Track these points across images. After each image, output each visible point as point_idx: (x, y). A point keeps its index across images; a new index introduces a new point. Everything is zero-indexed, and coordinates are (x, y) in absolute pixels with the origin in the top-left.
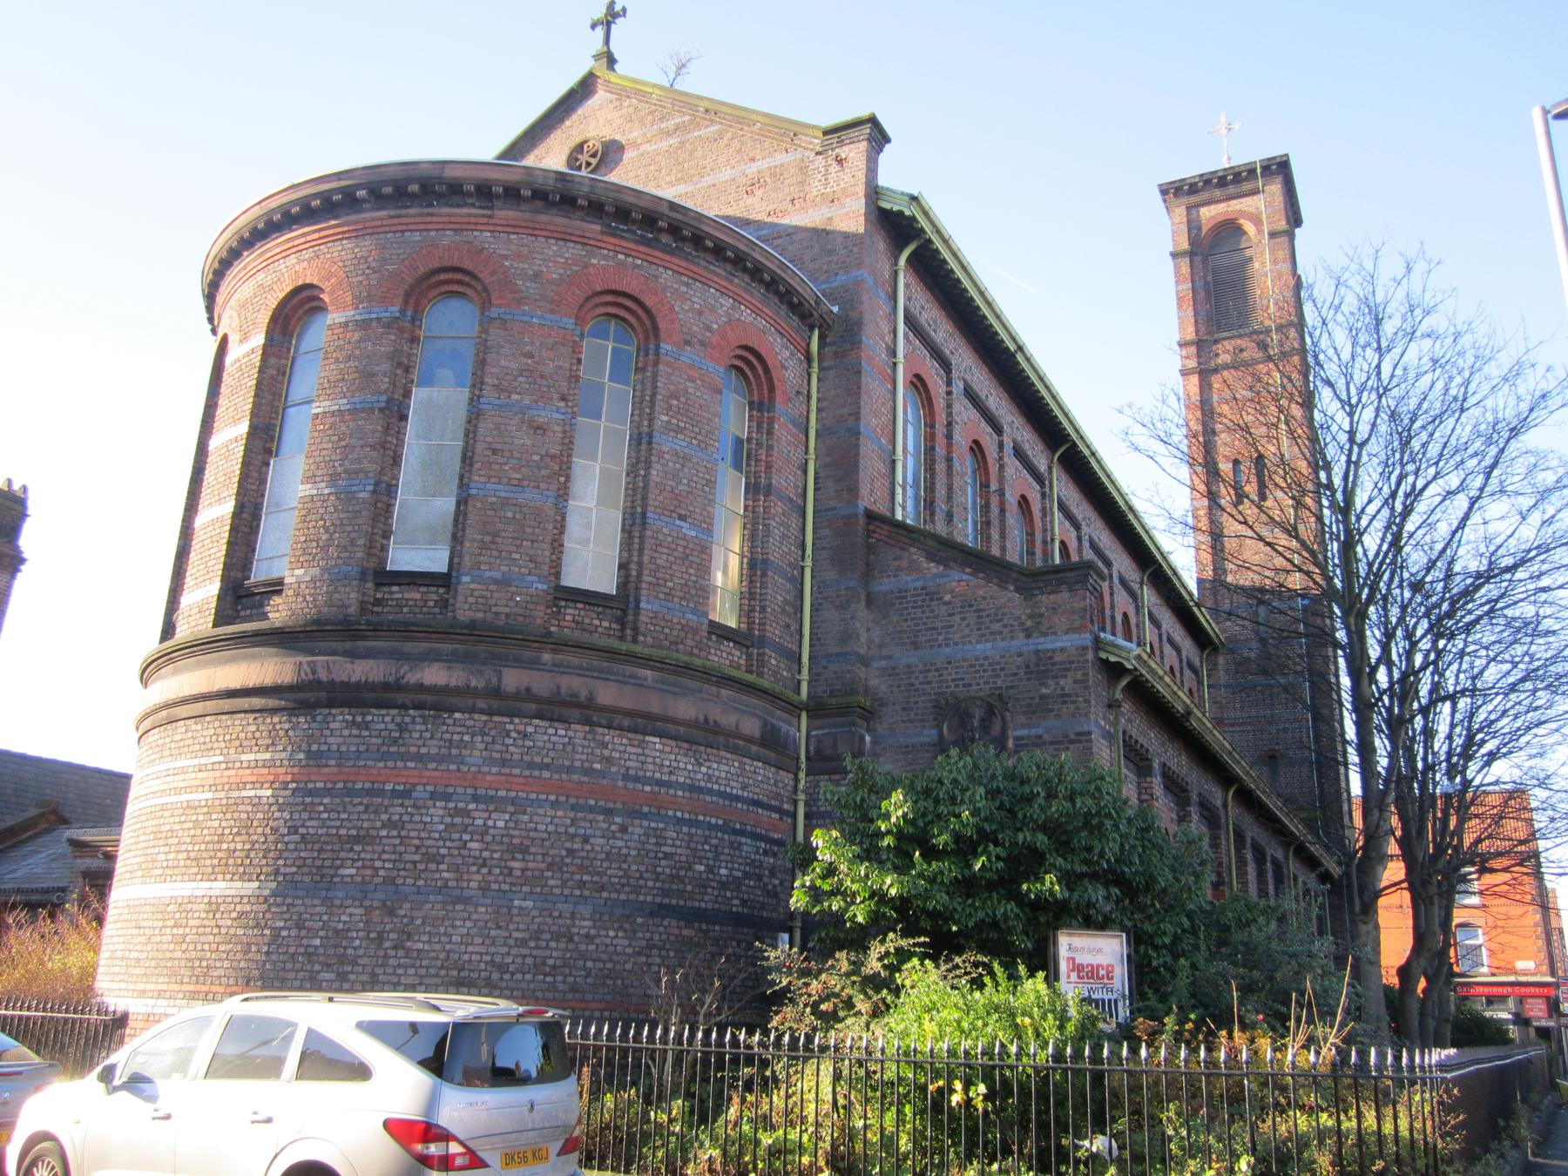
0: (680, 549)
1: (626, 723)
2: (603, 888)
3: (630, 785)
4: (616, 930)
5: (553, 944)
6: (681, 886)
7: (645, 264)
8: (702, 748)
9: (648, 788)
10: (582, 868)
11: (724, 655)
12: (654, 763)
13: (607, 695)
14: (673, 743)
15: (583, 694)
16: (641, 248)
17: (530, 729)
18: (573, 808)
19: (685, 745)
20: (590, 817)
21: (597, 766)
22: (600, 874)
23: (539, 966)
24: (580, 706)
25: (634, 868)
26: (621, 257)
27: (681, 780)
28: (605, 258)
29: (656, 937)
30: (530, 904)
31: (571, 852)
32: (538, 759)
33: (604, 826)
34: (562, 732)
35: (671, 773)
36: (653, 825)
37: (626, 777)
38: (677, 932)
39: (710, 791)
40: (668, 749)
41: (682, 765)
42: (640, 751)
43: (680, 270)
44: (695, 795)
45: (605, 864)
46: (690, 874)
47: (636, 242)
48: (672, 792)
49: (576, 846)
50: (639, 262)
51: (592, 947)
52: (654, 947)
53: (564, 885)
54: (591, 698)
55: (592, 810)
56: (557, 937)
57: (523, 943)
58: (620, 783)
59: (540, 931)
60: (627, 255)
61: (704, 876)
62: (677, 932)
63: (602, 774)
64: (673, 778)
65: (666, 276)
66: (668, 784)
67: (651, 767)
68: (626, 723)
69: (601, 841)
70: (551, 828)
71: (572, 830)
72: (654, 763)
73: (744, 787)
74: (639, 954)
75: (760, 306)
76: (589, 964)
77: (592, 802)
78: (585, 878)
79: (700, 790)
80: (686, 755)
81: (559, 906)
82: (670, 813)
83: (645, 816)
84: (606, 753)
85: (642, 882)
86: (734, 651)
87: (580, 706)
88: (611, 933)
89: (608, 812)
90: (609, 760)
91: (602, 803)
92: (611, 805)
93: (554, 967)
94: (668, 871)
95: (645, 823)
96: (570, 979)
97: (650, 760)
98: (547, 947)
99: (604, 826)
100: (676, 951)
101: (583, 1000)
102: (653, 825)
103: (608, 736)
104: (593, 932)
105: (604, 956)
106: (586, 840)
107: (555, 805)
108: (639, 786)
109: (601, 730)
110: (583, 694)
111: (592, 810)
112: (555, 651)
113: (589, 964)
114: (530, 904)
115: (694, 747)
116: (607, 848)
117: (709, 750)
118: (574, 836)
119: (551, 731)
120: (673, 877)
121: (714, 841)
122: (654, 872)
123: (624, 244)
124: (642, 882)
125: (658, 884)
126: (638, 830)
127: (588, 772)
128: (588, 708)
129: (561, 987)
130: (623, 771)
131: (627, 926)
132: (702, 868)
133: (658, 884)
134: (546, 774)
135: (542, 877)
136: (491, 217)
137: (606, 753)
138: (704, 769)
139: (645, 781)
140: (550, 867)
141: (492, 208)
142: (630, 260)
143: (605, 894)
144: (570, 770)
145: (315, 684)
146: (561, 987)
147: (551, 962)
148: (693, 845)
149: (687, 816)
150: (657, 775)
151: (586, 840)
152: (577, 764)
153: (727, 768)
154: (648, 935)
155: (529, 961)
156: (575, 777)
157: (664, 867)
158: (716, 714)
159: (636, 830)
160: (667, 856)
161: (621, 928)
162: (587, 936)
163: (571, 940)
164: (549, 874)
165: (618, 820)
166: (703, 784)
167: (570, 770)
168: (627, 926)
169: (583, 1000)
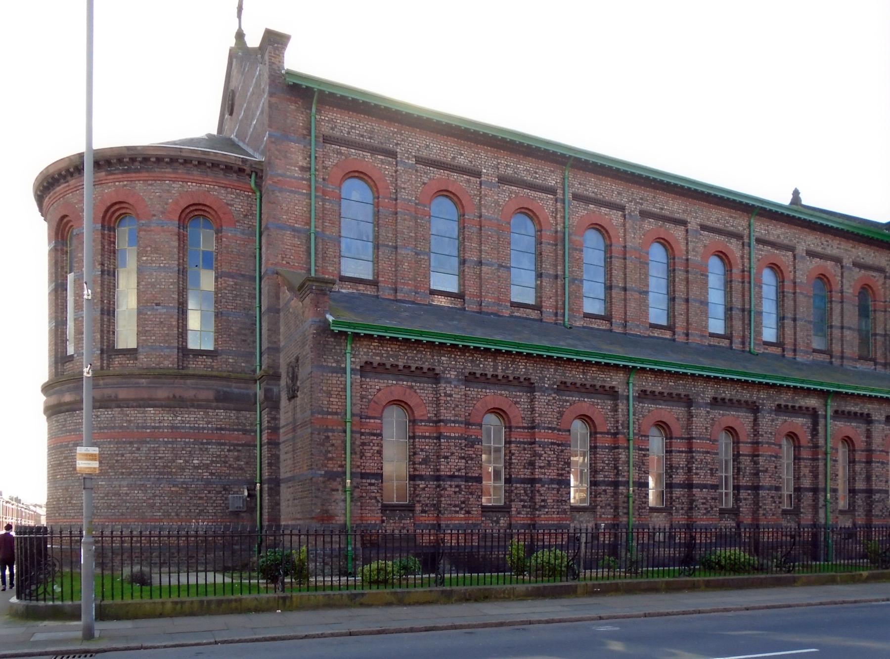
0: (158, 320)
1: (135, 404)
2: (131, 474)
3: (140, 430)
4: (138, 490)
5: (113, 498)
6: (169, 470)
7: (129, 183)
8: (177, 409)
9: (148, 431)
10: (123, 467)
11: (200, 363)
12: (151, 419)
13: (123, 394)
14: (160, 409)
15: (113, 395)
16: (125, 175)
17: (99, 413)
18: (117, 443)
19: (168, 409)
20: (123, 446)
21: (125, 424)
22: (130, 468)
23: (109, 507)
24: (113, 400)
25: (144, 464)
26: (117, 183)
27: (166, 425)
28: (109, 187)
29: (158, 492)
30: (103, 483)
31: (117, 461)
32: (102, 425)
33: (130, 449)
34: (110, 413)
35: (160, 422)
36: (152, 446)
37: (137, 428)
38: (169, 489)
39: (183, 428)
40: (158, 412)
41: (165, 418)
42: (143, 415)
43: (147, 179)
44: (174, 430)
45: (131, 464)
46: (174, 464)
47: (121, 173)
48: (161, 430)
49: (119, 458)
50: (125, 183)
51: (128, 498)
52: (157, 496)
53: (116, 474)
54: (116, 397)
55: (124, 442)
56: (115, 495)
57: (103, 498)
58: (135, 430)
59: (108, 493)
60: (120, 182)
61: (183, 465)
62: (169, 489)
63: (127, 427)
64: (162, 425)
65: (139, 185)
66: (159, 428)
67: (149, 421)
68: (135, 404)
69: (128, 455)
70: (109, 452)
71: (116, 452)
72: (151, 419)
73: (208, 423)
74: (149, 499)
75: (201, 179)
76: (128, 504)
77: (124, 440)
78: (124, 471)
79: (178, 428)
80: (168, 414)
81: (115, 483)
82: (161, 440)
83: (148, 443)
84: (128, 418)
85: (148, 470)
86: (206, 360)
87: (113, 400)
88: (136, 492)
89: (131, 443)
90: (130, 421)
91: (128, 440)
92: (132, 440)
93: (114, 506)
94: (162, 464)
95: (148, 446)
96: (121, 511)
97: (148, 418)
98: (111, 499)
99: (130, 449)
100: (169, 497)
101: (126, 518)
102: (152, 446)
103: (128, 411)
104: (128, 492)
105: (133, 501)
106: (123, 455)
107: (110, 443)
108: (144, 430)
109: (125, 409)
110: (113, 395)
111: (124, 442)
112: (103, 379)
113: (128, 504)
114: (103, 483)
115: (172, 409)
116: (131, 458)
117: (182, 409)
118: (118, 454)
119: (106, 413)
120: (164, 467)
121: (188, 449)
122: (154, 465)
123: (116, 176)
124: (148, 470)
125: (157, 470)
126: (145, 449)
127: (121, 427)
128: (117, 401)
129: (117, 514)
130: (136, 425)
131: (143, 488)
132: (182, 461)
133: (157, 470)
134: (106, 431)
135: (108, 472)
136: (68, 186)
137: (128, 418)
138: (179, 418)
139: (146, 428)
140: (110, 468)
141: (67, 182)
142: (121, 183)
143: (132, 476)
144: (114, 428)
145: (60, 405)
146: (117, 514)
147: (113, 504)
148: (175, 452)
149: (170, 440)
150: (153, 424)
151: (123, 455)
152: (117, 425)
153: (195, 416)
154: (153, 491)
155: (106, 504)
156: (116, 430)
157: (160, 463)
158: (179, 393)
159: (144, 449)
160: (160, 458)
161: (140, 489)
162: (126, 493)
163: (120, 495)
164: (109, 470)
165: (135, 445)
166: (179, 425)
167: (114, 428)
168: (143, 488)
169: (126, 518)
